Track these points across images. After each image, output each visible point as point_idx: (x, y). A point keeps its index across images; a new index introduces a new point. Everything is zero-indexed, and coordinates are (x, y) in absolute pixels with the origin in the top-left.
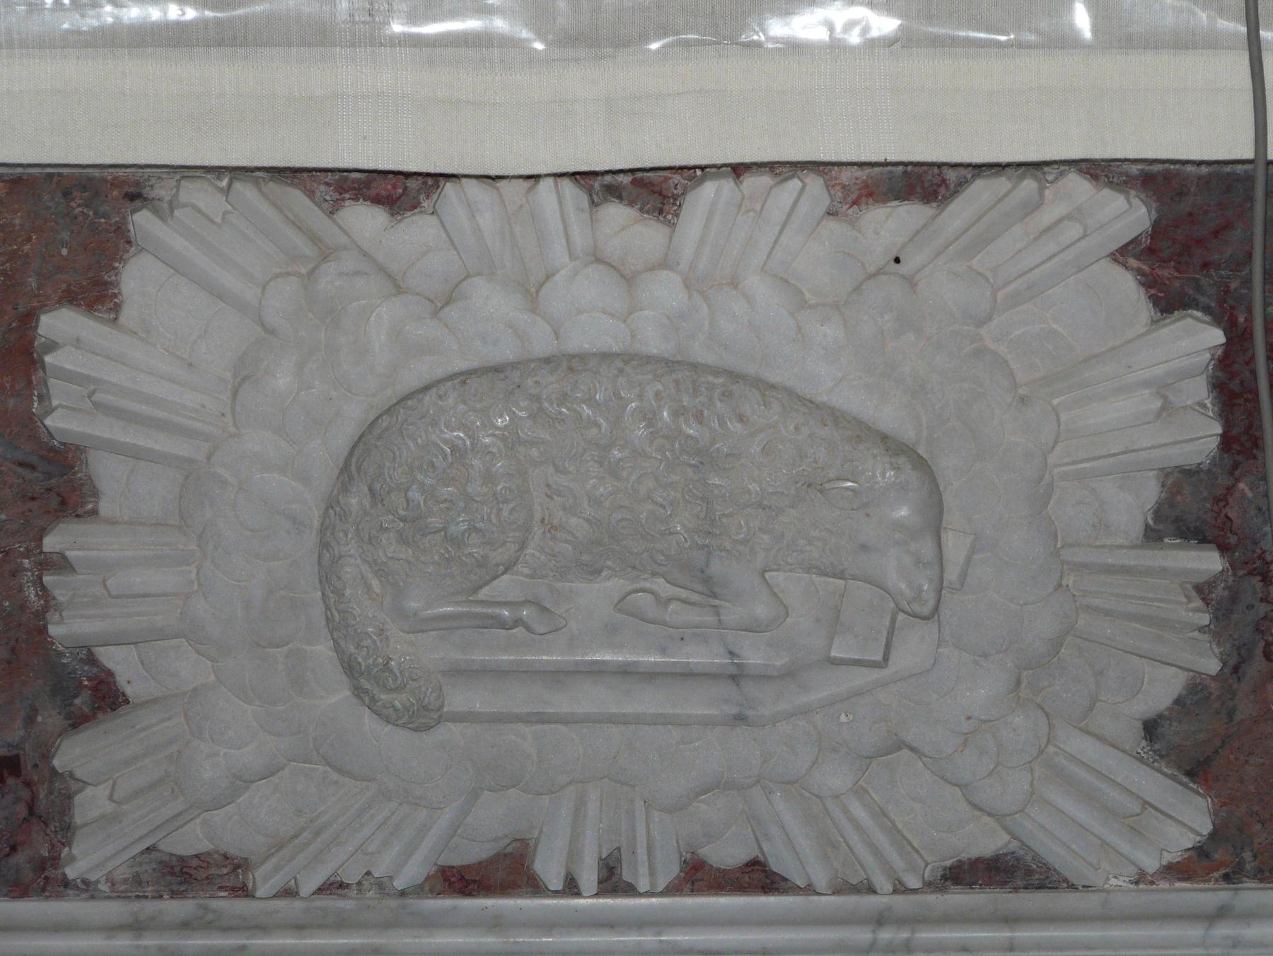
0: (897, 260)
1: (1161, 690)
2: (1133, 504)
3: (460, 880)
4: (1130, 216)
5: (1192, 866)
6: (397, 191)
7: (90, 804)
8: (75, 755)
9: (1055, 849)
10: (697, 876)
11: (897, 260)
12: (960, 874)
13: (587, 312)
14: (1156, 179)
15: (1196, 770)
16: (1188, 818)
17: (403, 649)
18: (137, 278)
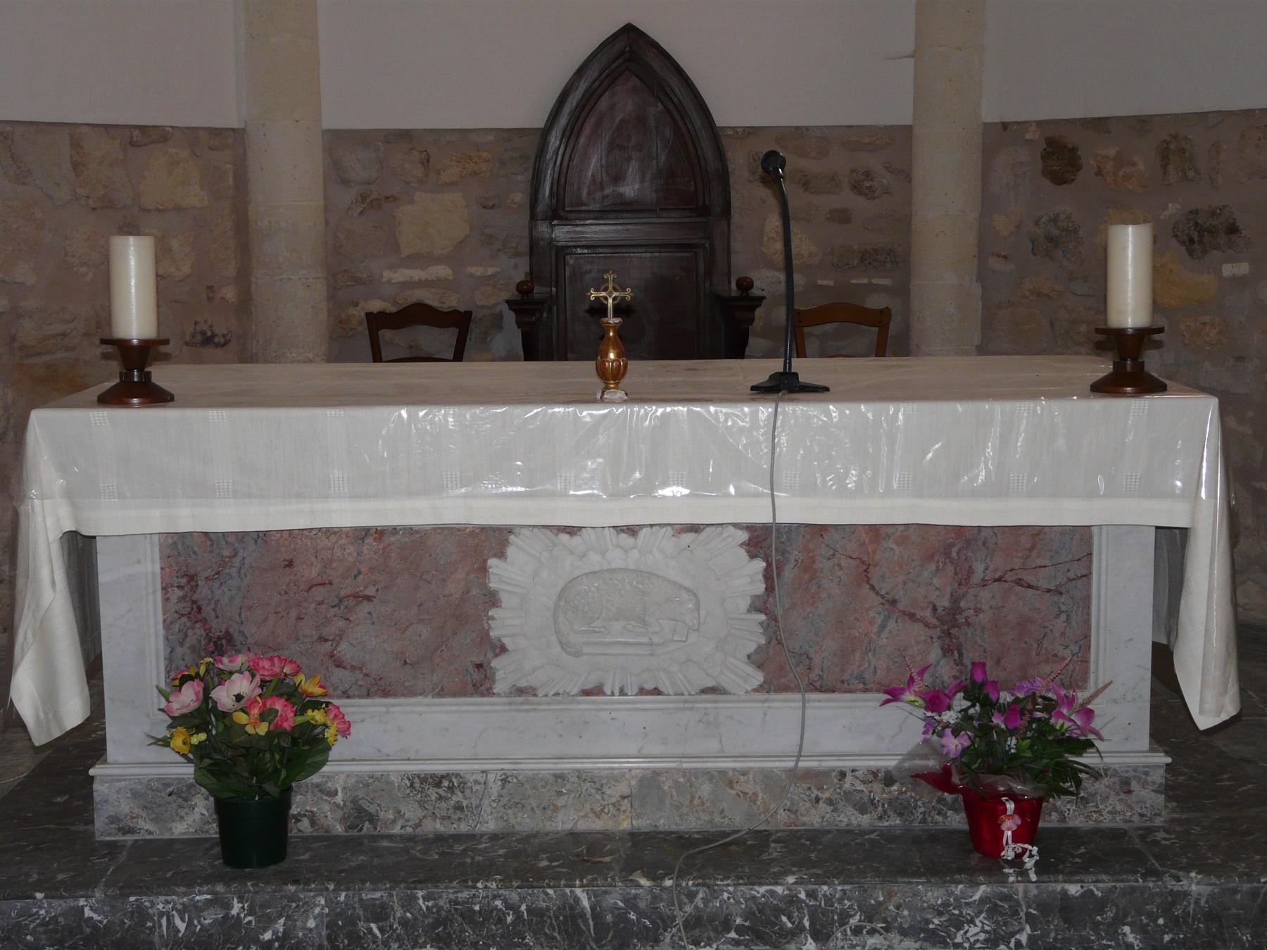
1: (751, 648)
2: (745, 603)
3: (586, 693)
4: (744, 536)
6: (571, 531)
7: (333, 754)
8: (495, 663)
10: (642, 691)
13: (616, 559)
14: (750, 528)
15: (760, 666)
16: (758, 677)
18: (510, 551)
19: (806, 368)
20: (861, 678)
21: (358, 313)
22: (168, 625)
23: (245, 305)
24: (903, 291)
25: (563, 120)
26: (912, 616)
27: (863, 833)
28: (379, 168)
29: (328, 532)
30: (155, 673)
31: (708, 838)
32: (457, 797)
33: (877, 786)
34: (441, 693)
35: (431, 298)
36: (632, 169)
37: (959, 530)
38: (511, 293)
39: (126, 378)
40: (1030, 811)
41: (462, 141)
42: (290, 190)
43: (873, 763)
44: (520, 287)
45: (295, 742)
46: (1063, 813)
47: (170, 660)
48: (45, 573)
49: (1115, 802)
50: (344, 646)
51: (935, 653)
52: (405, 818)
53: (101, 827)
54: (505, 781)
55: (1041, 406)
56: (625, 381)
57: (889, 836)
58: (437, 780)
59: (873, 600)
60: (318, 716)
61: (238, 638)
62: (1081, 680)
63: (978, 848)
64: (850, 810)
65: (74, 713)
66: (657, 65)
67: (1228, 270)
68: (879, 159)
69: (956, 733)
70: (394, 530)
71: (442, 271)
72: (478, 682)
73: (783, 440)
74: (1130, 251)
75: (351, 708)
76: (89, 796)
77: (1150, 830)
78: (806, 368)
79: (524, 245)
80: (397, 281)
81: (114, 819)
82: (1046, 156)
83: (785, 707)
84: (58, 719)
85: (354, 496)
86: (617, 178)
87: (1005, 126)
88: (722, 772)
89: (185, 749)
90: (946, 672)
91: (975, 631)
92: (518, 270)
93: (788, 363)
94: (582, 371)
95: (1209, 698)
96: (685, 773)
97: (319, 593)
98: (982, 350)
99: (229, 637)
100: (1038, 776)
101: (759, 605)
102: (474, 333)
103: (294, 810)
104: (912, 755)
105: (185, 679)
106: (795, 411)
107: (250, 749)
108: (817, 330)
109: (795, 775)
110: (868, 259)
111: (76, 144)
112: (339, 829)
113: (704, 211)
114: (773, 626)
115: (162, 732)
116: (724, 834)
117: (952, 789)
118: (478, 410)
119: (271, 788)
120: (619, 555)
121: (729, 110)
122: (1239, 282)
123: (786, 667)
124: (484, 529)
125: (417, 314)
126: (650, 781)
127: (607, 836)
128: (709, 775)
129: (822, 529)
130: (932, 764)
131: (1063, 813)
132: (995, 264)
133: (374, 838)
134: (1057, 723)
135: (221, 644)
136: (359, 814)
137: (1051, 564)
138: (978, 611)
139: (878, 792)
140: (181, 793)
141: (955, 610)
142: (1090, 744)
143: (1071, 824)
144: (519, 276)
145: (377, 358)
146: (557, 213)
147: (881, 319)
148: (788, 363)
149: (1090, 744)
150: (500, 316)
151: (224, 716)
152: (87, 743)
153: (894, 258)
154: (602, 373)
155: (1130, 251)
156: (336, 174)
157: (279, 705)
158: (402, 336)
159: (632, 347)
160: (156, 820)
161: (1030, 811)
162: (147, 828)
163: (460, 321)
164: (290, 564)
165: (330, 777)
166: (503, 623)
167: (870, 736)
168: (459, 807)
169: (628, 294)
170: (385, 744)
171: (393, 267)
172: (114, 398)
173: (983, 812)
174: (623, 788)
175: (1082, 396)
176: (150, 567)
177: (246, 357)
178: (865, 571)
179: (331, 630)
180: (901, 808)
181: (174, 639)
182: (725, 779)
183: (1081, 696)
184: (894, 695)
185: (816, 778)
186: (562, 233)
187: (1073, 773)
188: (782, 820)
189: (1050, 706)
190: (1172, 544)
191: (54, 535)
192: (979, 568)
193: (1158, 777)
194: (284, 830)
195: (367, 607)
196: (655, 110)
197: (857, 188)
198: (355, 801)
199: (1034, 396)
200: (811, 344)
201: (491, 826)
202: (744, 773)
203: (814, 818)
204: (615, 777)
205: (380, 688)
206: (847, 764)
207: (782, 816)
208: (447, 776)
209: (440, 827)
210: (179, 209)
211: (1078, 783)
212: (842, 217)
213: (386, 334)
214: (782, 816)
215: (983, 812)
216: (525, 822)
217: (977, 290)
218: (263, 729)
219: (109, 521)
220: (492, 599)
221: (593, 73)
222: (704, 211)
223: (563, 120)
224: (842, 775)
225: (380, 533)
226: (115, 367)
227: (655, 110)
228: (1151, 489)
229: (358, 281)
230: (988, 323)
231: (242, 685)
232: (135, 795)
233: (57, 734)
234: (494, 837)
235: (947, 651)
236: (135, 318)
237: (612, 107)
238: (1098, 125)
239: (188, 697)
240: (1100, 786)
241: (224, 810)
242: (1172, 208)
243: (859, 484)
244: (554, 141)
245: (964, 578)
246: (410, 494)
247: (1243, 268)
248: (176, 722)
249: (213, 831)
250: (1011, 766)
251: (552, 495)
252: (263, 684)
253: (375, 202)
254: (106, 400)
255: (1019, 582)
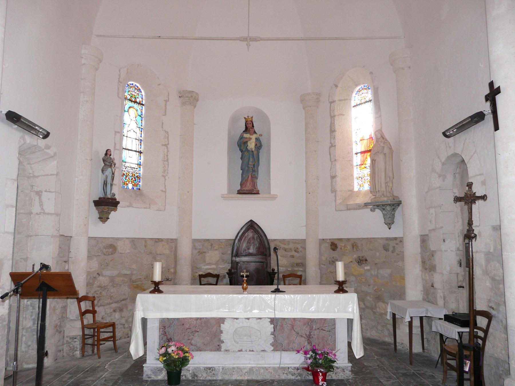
0: (409, 67)
1: (271, 342)
2: (270, 333)
3: (239, 351)
4: (270, 320)
5: (273, 350)
6: (237, 319)
7: (190, 363)
8: (222, 345)
9: (266, 350)
10: (250, 351)
11: (409, 67)
12: (163, 123)
13: (245, 324)
14: (271, 318)
15: (273, 346)
16: (272, 348)
17: (237, 340)
18: (225, 322)
19: (281, 287)
20: (292, 348)
21: (197, 274)
22: (160, 336)
23: (175, 273)
24: (305, 271)
25: (238, 238)
26: (302, 336)
27: (293, 380)
28: (202, 246)
29: (191, 318)
30: (156, 345)
31: (262, 381)
32: (214, 372)
33: (296, 370)
34: (211, 351)
35: (211, 272)
36: (252, 247)
37: (310, 319)
38: (227, 271)
39: (155, 288)
40: (324, 375)
41: (219, 241)
42: (185, 250)
43: (295, 366)
44: (229, 270)
45: (183, 360)
46: (331, 376)
47: (160, 343)
48: (138, 326)
49: (341, 374)
50: (193, 341)
51: (306, 343)
52: (203, 376)
53: (145, 377)
54: (223, 369)
55: (324, 295)
56: (247, 290)
57: (298, 381)
58: (210, 368)
59: (294, 333)
60: (187, 355)
61: (173, 339)
62: (334, 349)
63: (315, 383)
64: (290, 375)
65: (141, 353)
66: (256, 227)
67: (366, 268)
68: (299, 246)
69: (310, 359)
70: (203, 318)
71: (214, 266)
72: (218, 349)
73: (276, 302)
74: (340, 267)
75: (194, 353)
76: (143, 371)
77: (348, 379)
78: (281, 287)
79: (230, 262)
80: (205, 269)
81: (147, 375)
82: (331, 245)
83: (277, 354)
84: (138, 355)
85: (196, 311)
86: (249, 249)
87: (323, 239)
88: (265, 367)
89: (162, 361)
90: (309, 347)
91: (313, 339)
92: (229, 266)
93: (278, 287)
94: (239, 288)
95: (359, 353)
96: (258, 367)
97: (188, 330)
98: (321, 284)
99: (171, 339)
100: (326, 368)
101: (273, 334)
102: (220, 279)
103: (182, 374)
104: (301, 364)
105: (163, 347)
106: (279, 296)
107: (174, 361)
108: (288, 279)
109: (280, 368)
110: (298, 265)
111: (146, 242)
112: (190, 378)
113: (266, 255)
114: (275, 338)
115: (158, 357)
116: (265, 380)
117: (309, 371)
118: (220, 295)
119: (178, 369)
120: (246, 324)
121: (271, 235)
122: (368, 270)
123: (278, 346)
124: (220, 318)
125: (209, 275)
126: (251, 369)
127: (242, 380)
128: (263, 368)
129: (284, 319)
130: (306, 366)
131: (331, 376)
132: (322, 266)
133: (197, 380)
134: (329, 357)
135: (169, 340)
136: (194, 375)
137: (327, 326)
138: (314, 335)
139: (296, 372)
140: (160, 370)
141: (310, 335)
142: (335, 361)
143: (333, 378)
144: (229, 268)
145: (201, 284)
146: (237, 255)
147: (300, 277)
148: (278, 287)
149: (335, 361)
150: (225, 276)
151: (170, 354)
152: (142, 360)
153: (303, 265)
154: (243, 288)
155: (340, 267)
156: (194, 247)
157: (180, 352)
158: (206, 279)
159: (249, 283)
160: (155, 375)
161: (324, 375)
162: (154, 377)
163: (217, 276)
164: (183, 324)
165: (189, 367)
166: (223, 337)
167: (294, 360)
168: (214, 374)
169: (248, 274)
170: (200, 361)
171: (204, 265)
172: (152, 292)
173: (315, 375)
174: (246, 371)
175: (332, 293)
176: (157, 325)
177: (175, 284)
178: (293, 327)
179: (190, 338)
180: (300, 375)
181: (161, 339)
182: (266, 369)
183: (334, 352)
184: (298, 352)
185: (283, 369)
186: (238, 259)
187: (332, 367)
188: (277, 377)
189: (328, 354)
190: (350, 322)
191: (140, 318)
192: (314, 327)
193: (350, 368)
194: (180, 378)
195: (197, 333)
196: (256, 236)
197: (295, 251)
198: (194, 372)
199: (323, 293)
200: (287, 282)
201: (220, 378)
202: (270, 367)
203: (283, 377)
204: (244, 368)
205: (199, 350)
206: (290, 366)
207: (277, 377)
208: (212, 368)
209: (210, 378)
210: (164, 254)
211: (333, 369)
212: (293, 257)
213: (202, 279)
214: (277, 377)
215: (315, 375)
216: (227, 377)
217: (319, 271)
218: (177, 357)
219: (150, 316)
220: (221, 332)
221: (244, 229)
222: (266, 255)
223: (238, 238)
224: (289, 368)
225: (201, 319)
226: (153, 286)
227: (256, 236)
228: (346, 312)
229: (198, 268)
230: (321, 277)
231: (173, 348)
232: (152, 370)
233: (138, 357)
234: (221, 380)
235: (308, 343)
236: (157, 278)
237: (248, 235)
238: (340, 240)
239: (163, 350)
240: (338, 370)
241: (169, 374)
242: (355, 256)
243: (291, 310)
244: (237, 241)
245: (311, 329)
246: (207, 311)
247: (368, 268)
248: (161, 355)
249: (166, 378)
250: (321, 366)
251: (233, 312)
252: (177, 348)
253: (202, 253)
254: (152, 292)
255: (322, 329)
